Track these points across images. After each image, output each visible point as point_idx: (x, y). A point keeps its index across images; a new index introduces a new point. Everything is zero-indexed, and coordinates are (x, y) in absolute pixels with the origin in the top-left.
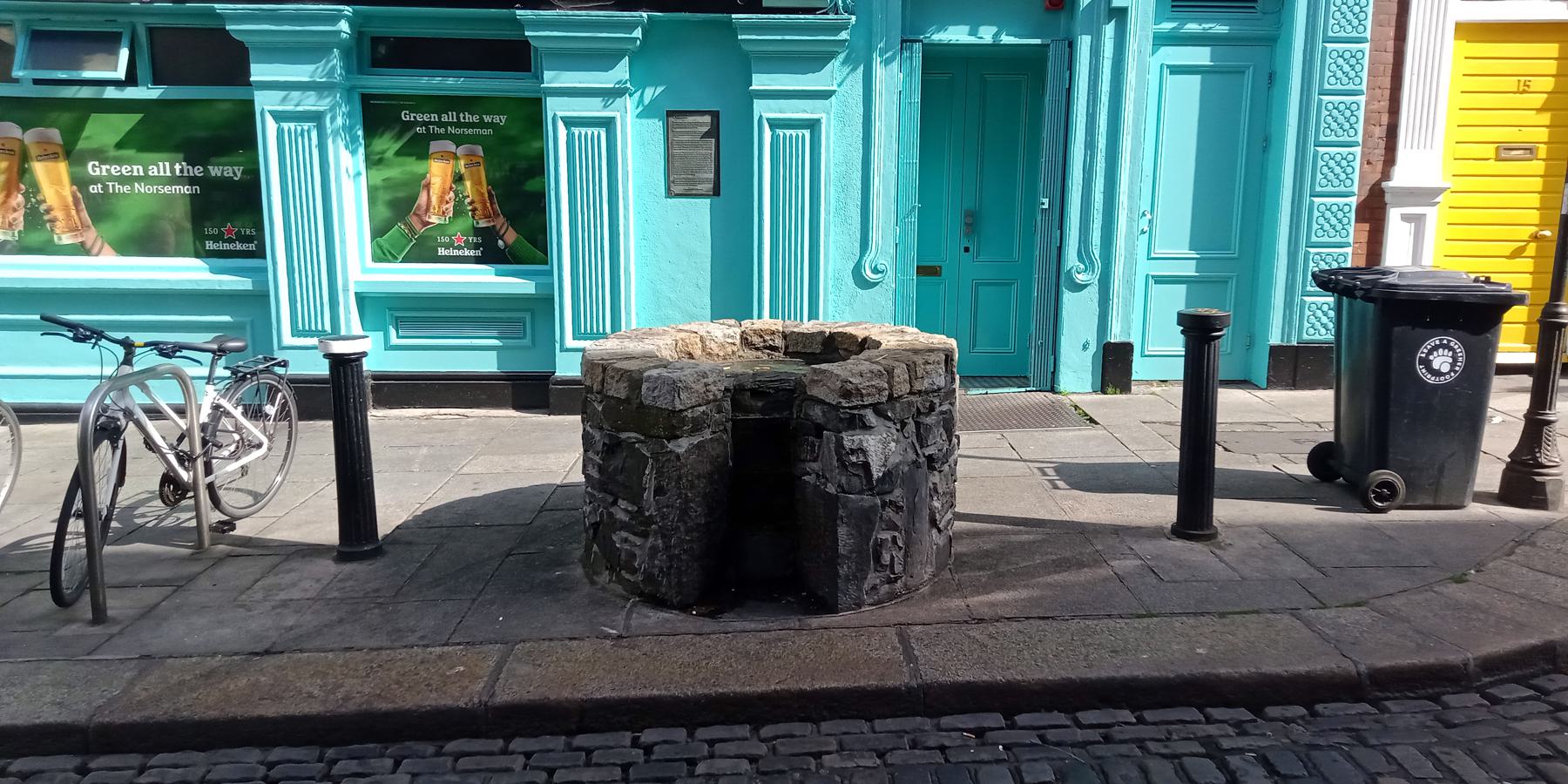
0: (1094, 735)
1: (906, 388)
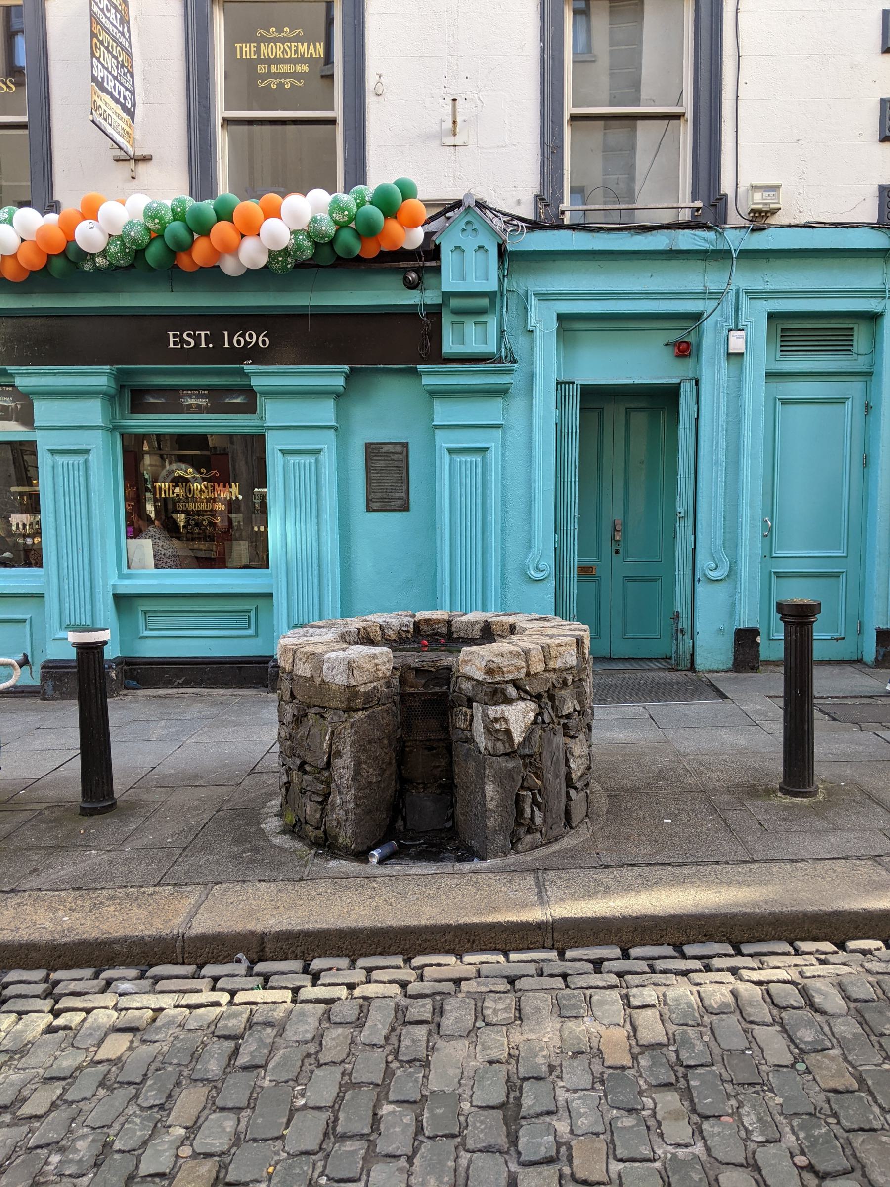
0: (697, 964)
1: (540, 667)
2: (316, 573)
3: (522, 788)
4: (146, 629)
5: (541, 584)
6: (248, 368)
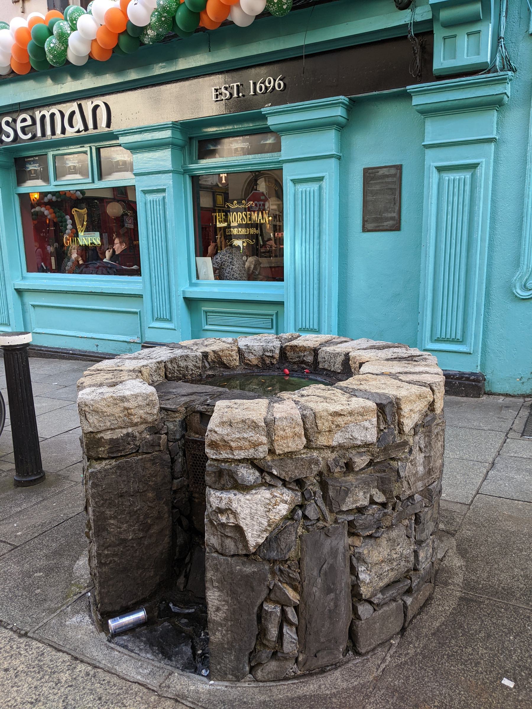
2: (316, 286)
3: (268, 599)
4: (207, 324)
5: (522, 304)
6: (265, 110)
